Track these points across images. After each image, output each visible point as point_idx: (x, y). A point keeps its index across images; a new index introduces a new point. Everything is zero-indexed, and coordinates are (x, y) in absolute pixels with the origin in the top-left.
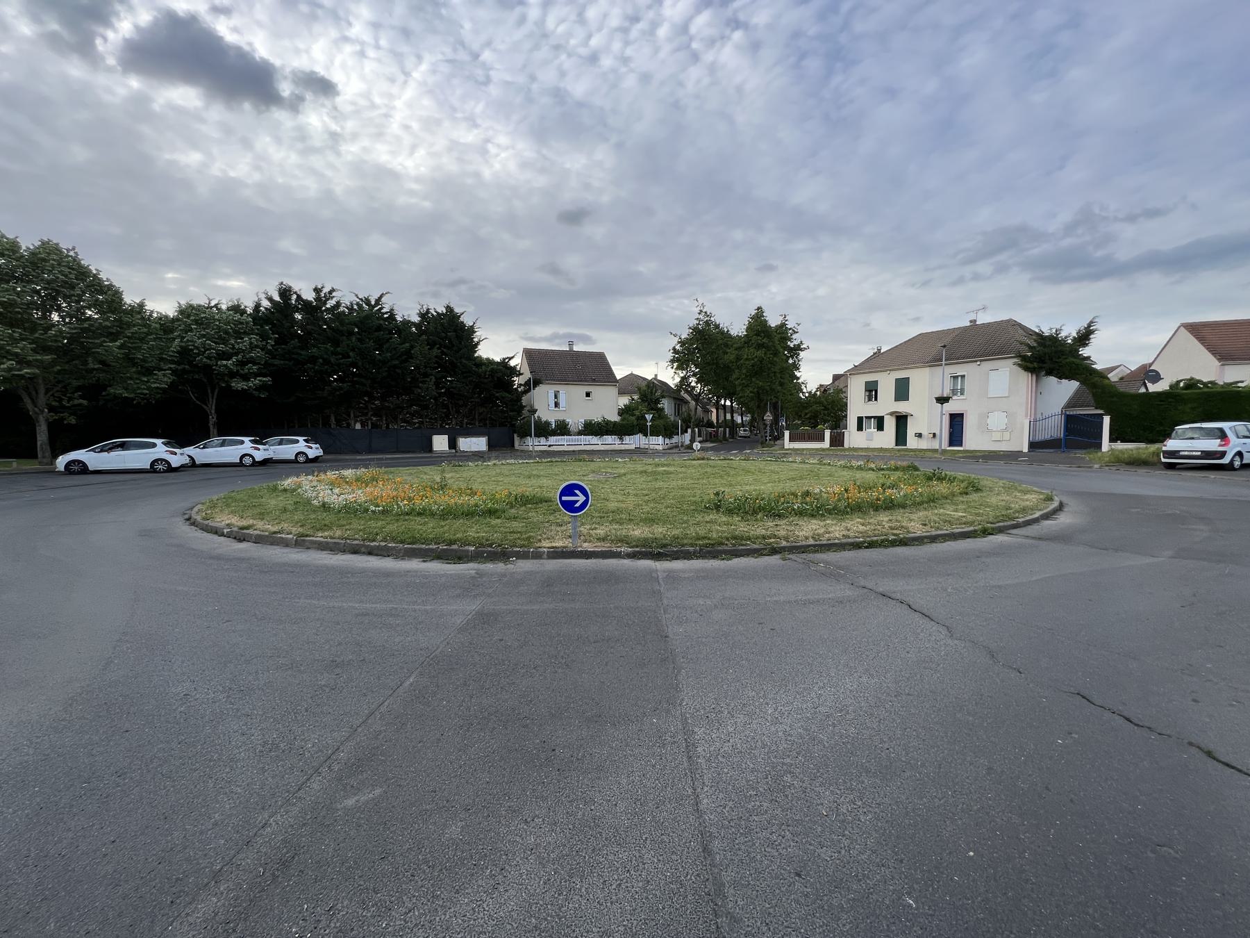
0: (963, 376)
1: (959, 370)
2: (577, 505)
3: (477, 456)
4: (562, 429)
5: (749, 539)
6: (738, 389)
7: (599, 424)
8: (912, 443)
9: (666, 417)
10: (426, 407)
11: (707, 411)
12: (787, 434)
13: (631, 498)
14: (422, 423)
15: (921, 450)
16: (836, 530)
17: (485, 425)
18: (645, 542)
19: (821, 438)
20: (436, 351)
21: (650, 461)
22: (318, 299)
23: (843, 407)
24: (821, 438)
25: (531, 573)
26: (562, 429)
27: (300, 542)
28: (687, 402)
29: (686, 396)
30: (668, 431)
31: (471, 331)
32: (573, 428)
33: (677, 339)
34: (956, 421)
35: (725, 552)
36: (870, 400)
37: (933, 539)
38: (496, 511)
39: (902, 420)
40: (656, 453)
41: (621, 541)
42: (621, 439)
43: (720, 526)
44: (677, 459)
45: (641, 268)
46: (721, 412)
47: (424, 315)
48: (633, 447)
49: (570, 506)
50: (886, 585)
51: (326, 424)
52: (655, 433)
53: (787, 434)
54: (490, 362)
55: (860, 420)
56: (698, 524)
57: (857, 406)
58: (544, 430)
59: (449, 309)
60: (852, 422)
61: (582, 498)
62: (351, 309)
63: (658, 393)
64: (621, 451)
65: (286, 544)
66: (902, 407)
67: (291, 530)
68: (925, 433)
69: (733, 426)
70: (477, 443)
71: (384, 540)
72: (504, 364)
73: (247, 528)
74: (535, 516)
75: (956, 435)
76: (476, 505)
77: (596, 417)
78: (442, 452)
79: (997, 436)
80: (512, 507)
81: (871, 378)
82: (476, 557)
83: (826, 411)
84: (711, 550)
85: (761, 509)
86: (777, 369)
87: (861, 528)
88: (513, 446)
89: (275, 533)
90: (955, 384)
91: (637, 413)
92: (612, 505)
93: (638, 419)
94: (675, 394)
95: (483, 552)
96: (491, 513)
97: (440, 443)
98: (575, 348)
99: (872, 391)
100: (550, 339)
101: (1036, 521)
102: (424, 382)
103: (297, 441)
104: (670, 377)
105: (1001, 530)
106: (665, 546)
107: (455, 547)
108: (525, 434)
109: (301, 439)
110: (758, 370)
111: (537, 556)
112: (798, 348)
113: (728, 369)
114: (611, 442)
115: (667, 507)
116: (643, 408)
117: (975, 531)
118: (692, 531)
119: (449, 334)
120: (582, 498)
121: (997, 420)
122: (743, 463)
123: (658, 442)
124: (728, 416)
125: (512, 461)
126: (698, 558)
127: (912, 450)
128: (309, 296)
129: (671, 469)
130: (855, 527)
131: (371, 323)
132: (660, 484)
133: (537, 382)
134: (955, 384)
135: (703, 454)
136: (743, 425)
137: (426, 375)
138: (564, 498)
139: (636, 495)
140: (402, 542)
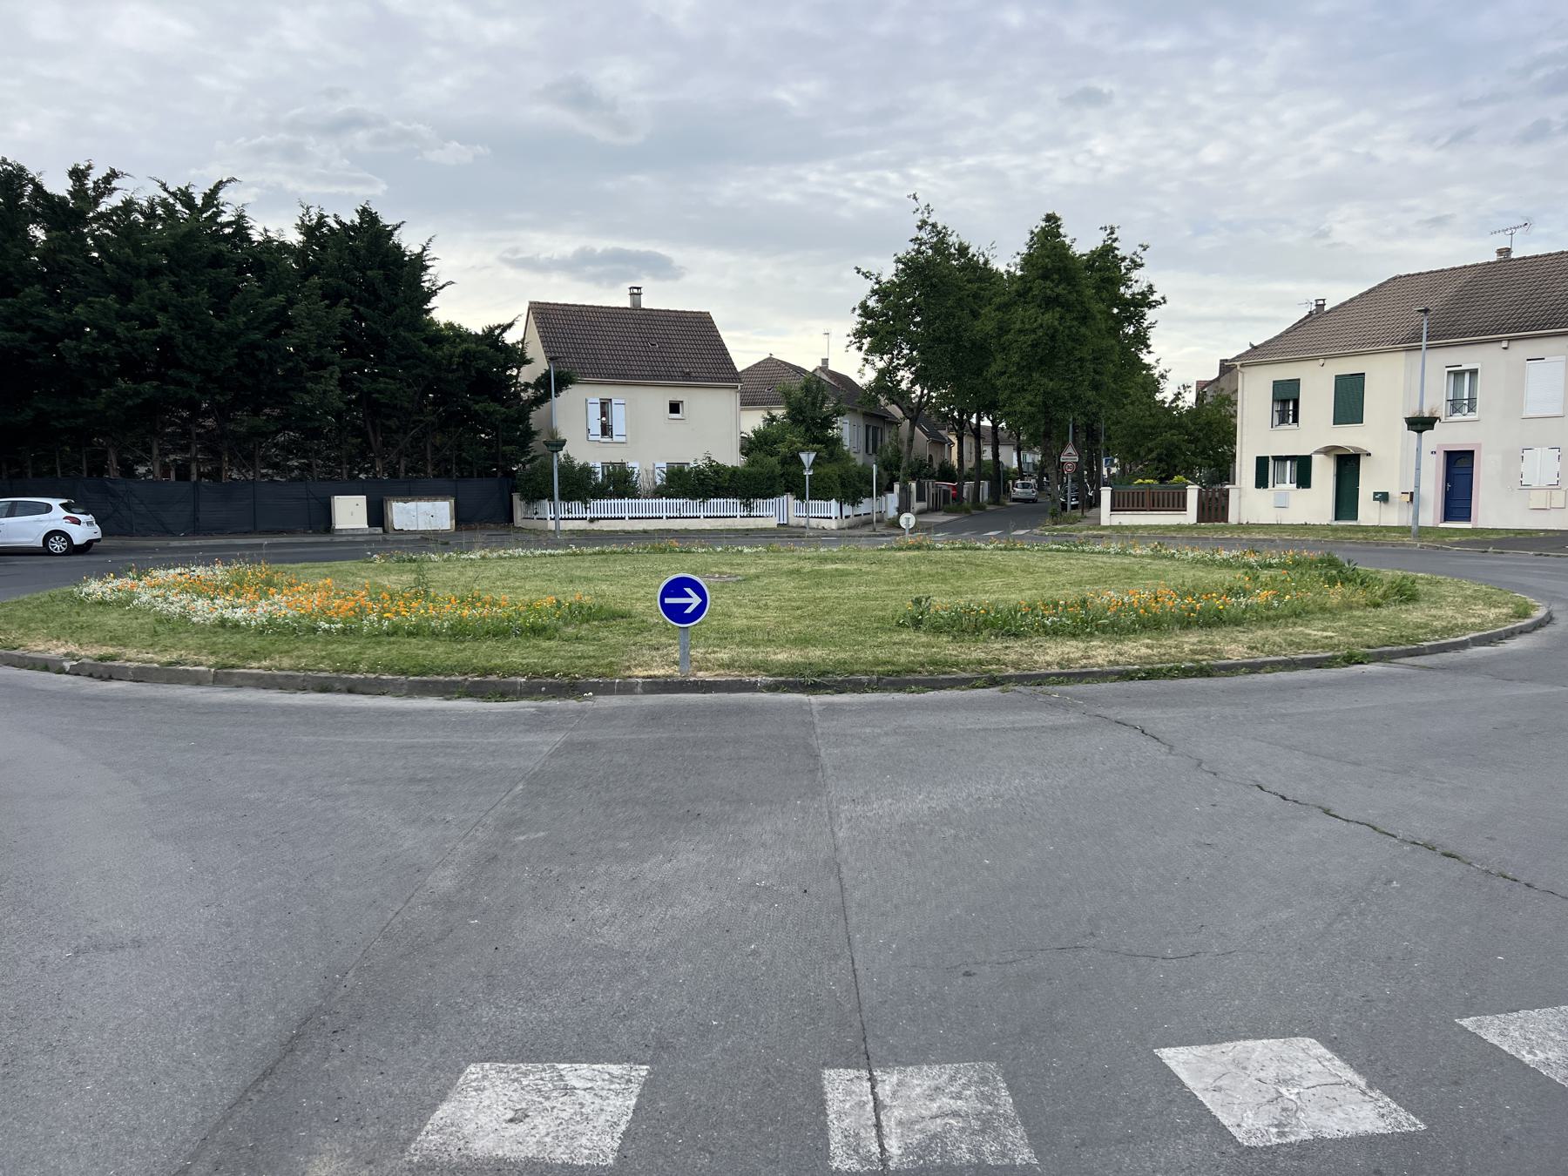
0: (1474, 372)
1: (1466, 358)
2: (688, 611)
3: (427, 540)
4: (620, 483)
5: (957, 664)
6: (1002, 397)
7: (699, 472)
8: (1369, 513)
9: (845, 457)
10: (315, 434)
11: (940, 443)
12: (1106, 494)
13: (772, 614)
14: (307, 468)
15: (1389, 529)
16: (1102, 653)
17: (448, 472)
18: (794, 669)
19: (1181, 506)
20: (342, 311)
21: (810, 552)
22: (79, 192)
23: (1230, 437)
24: (1181, 506)
25: (624, 708)
26: (620, 483)
27: (222, 677)
28: (894, 423)
29: (895, 410)
30: (850, 488)
31: (418, 264)
32: (643, 483)
33: (870, 285)
34: (1459, 465)
35: (917, 682)
36: (1283, 421)
37: (1254, 668)
38: (544, 628)
39: (1348, 464)
40: (823, 536)
41: (757, 667)
42: (748, 506)
43: (913, 648)
44: (866, 550)
45: (782, 95)
46: (969, 442)
47: (311, 231)
48: (772, 523)
49: (676, 613)
50: (1125, 714)
51: (98, 469)
52: (821, 491)
53: (1106, 494)
54: (456, 335)
55: (1262, 463)
56: (880, 646)
57: (1257, 434)
58: (579, 486)
59: (365, 213)
60: (1245, 470)
61: (695, 600)
62: (150, 215)
63: (829, 406)
64: (747, 532)
65: (197, 680)
66: (1348, 437)
67: (206, 663)
68: (1394, 492)
69: (999, 478)
70: (433, 514)
71: (372, 670)
72: (491, 338)
73: (112, 658)
74: (613, 636)
75: (1457, 500)
76: (509, 619)
77: (693, 457)
78: (354, 533)
79: (1538, 499)
80: (566, 625)
81: (1285, 373)
82: (529, 692)
83: (1194, 448)
84: (895, 679)
85: (987, 624)
86: (1085, 352)
87: (1144, 651)
88: (511, 519)
89: (170, 664)
90: (1457, 387)
91: (782, 449)
92: (740, 623)
93: (784, 462)
94: (868, 405)
95: (540, 685)
96: (537, 631)
97: (350, 512)
98: (646, 303)
99: (1287, 402)
100: (576, 265)
101: (1463, 645)
102: (316, 380)
103: (49, 508)
104: (857, 368)
105: (1380, 658)
106: (824, 673)
107: (493, 678)
108: (537, 492)
109: (55, 503)
110: (1046, 355)
111: (627, 688)
112: (1144, 301)
113: (981, 350)
114: (724, 513)
115: (831, 626)
116: (795, 437)
117: (1335, 657)
118: (868, 655)
119: (366, 270)
120: (695, 600)
121: (1541, 466)
122: (998, 556)
123: (828, 515)
124: (987, 455)
125: (519, 552)
126: (874, 690)
127: (1365, 529)
128: (59, 186)
129: (852, 567)
130: (1137, 649)
131: (191, 249)
132: (826, 592)
133: (564, 381)
134: (1457, 387)
135: (920, 537)
136: (1020, 474)
137: (320, 364)
138: (667, 601)
139: (780, 608)
140: (403, 673)
